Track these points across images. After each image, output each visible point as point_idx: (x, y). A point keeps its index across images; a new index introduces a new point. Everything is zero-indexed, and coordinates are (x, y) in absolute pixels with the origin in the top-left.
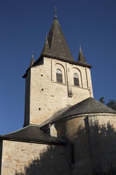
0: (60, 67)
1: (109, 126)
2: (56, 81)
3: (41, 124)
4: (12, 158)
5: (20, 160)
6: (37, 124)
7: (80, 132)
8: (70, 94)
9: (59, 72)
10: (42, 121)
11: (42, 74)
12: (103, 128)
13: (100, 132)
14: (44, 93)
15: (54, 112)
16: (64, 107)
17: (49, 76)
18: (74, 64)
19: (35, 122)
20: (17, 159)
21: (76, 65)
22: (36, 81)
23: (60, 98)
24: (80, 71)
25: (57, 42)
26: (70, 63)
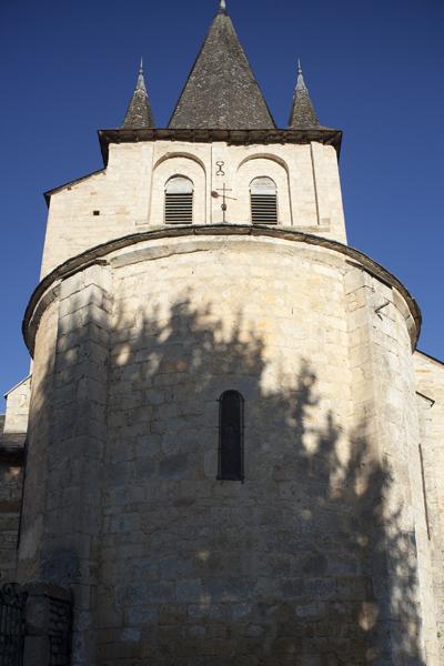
0: (186, 167)
1: (183, 318)
9: (180, 187)
11: (97, 209)
12: (144, 330)
18: (251, 143)
21: (264, 141)
22: (70, 240)
24: (283, 164)
26: (232, 140)
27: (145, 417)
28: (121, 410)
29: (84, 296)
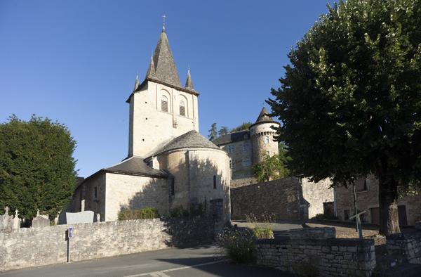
2: (161, 109)
7: (181, 166)
8: (175, 125)
9: (165, 99)
13: (199, 166)
21: (183, 91)
25: (164, 63)
29: (194, 156)
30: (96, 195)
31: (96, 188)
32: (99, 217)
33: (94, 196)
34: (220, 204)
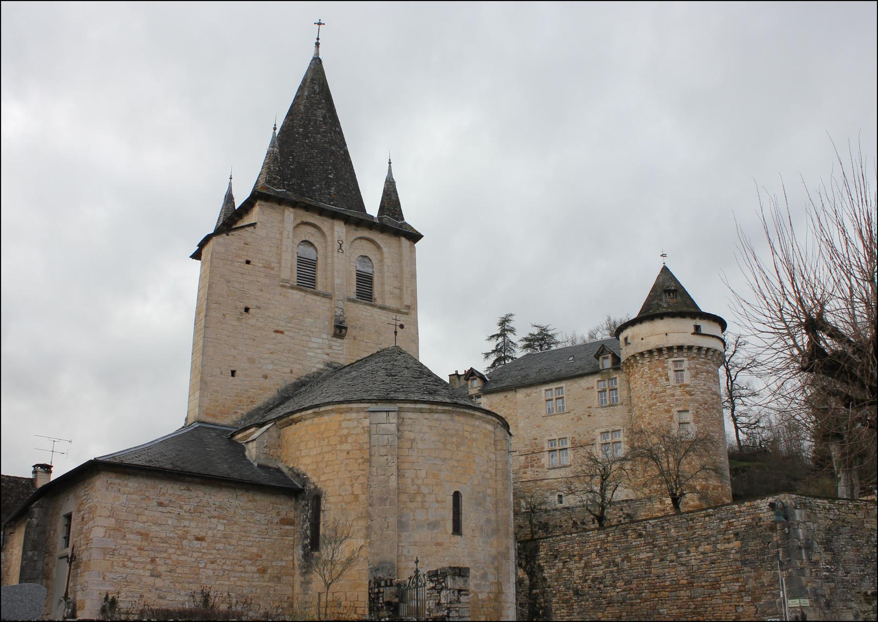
3: (236, 423)
4: (126, 525)
5: (151, 534)
6: (223, 423)
8: (340, 330)
9: (309, 253)
10: (240, 412)
11: (250, 259)
14: (252, 321)
15: (282, 385)
16: (314, 370)
17: (273, 265)
19: (214, 416)
20: (143, 531)
22: (229, 282)
23: (304, 338)
27: (419, 499)
28: (406, 493)
30: (67, 538)
31: (69, 517)
32: (464, 593)
33: (61, 542)
34: (459, 583)
